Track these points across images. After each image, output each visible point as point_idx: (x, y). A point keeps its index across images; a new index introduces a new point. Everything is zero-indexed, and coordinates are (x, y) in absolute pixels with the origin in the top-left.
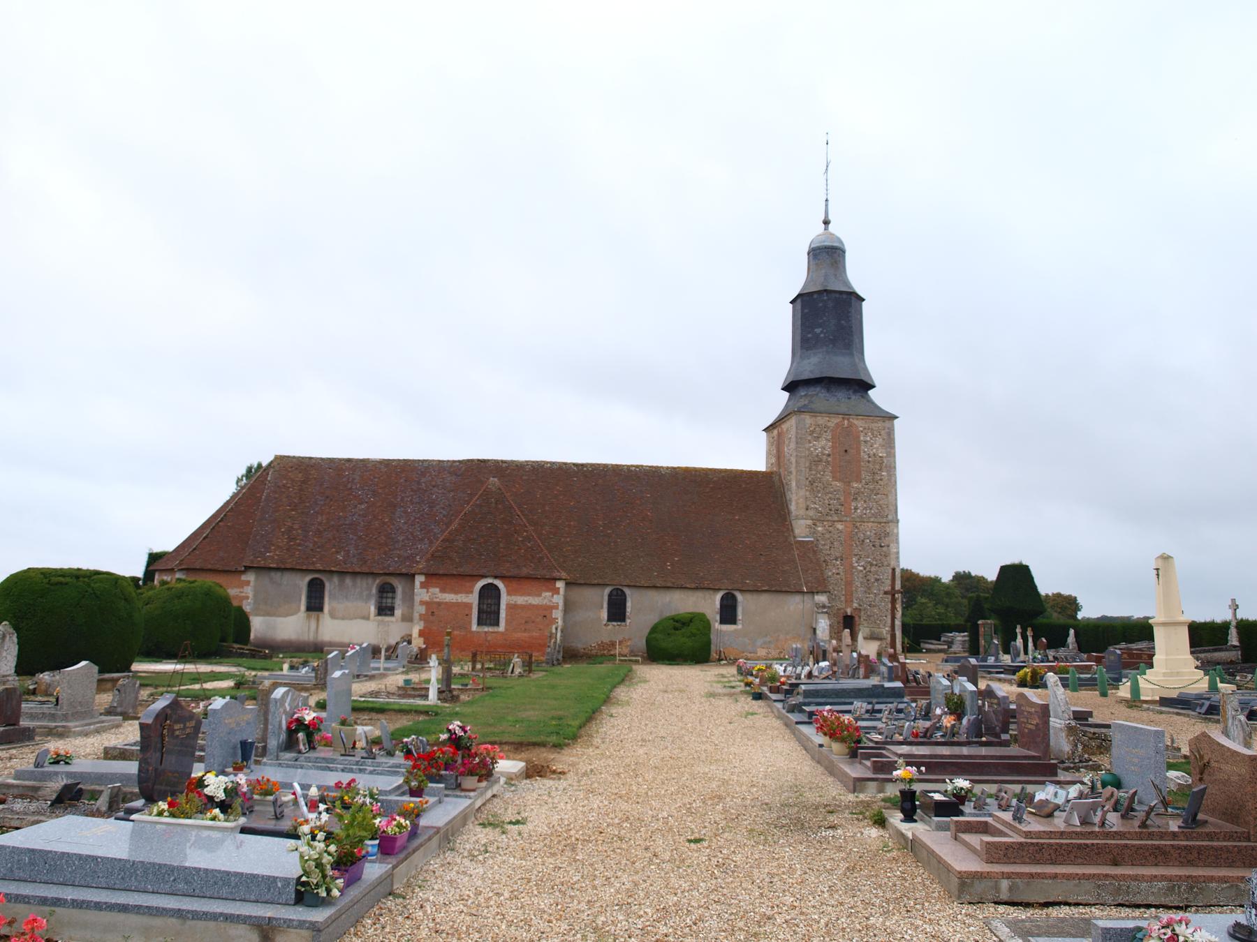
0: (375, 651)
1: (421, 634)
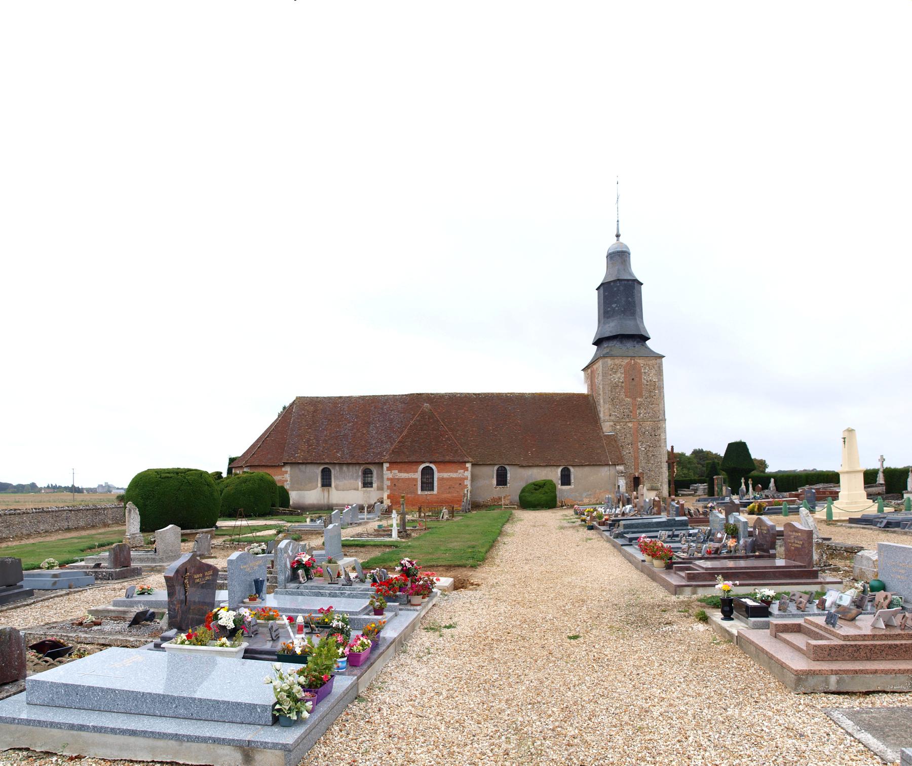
0: (361, 508)
1: (389, 497)
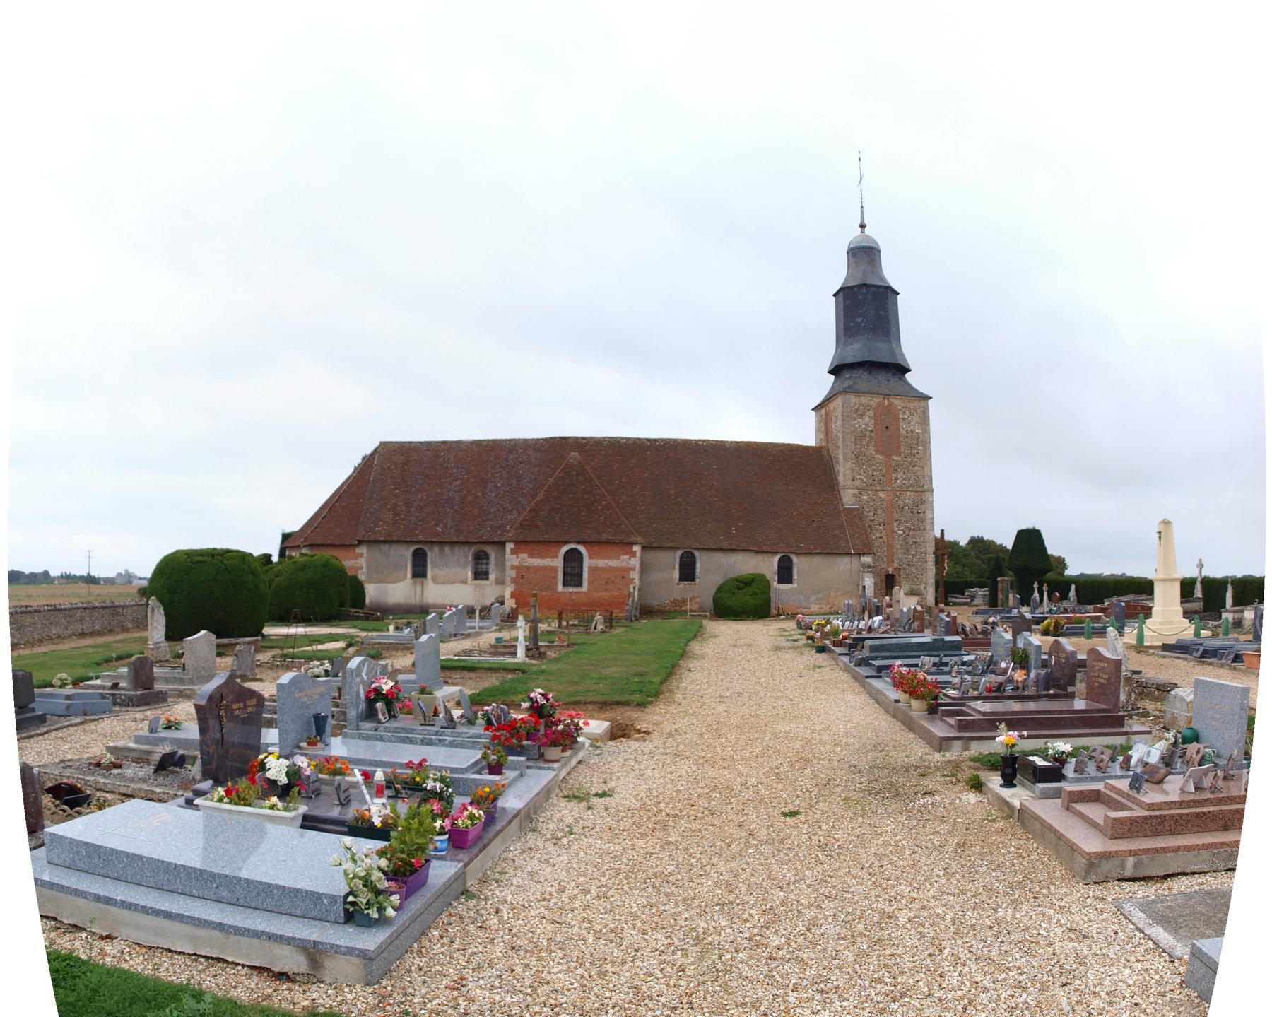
0: (470, 612)
